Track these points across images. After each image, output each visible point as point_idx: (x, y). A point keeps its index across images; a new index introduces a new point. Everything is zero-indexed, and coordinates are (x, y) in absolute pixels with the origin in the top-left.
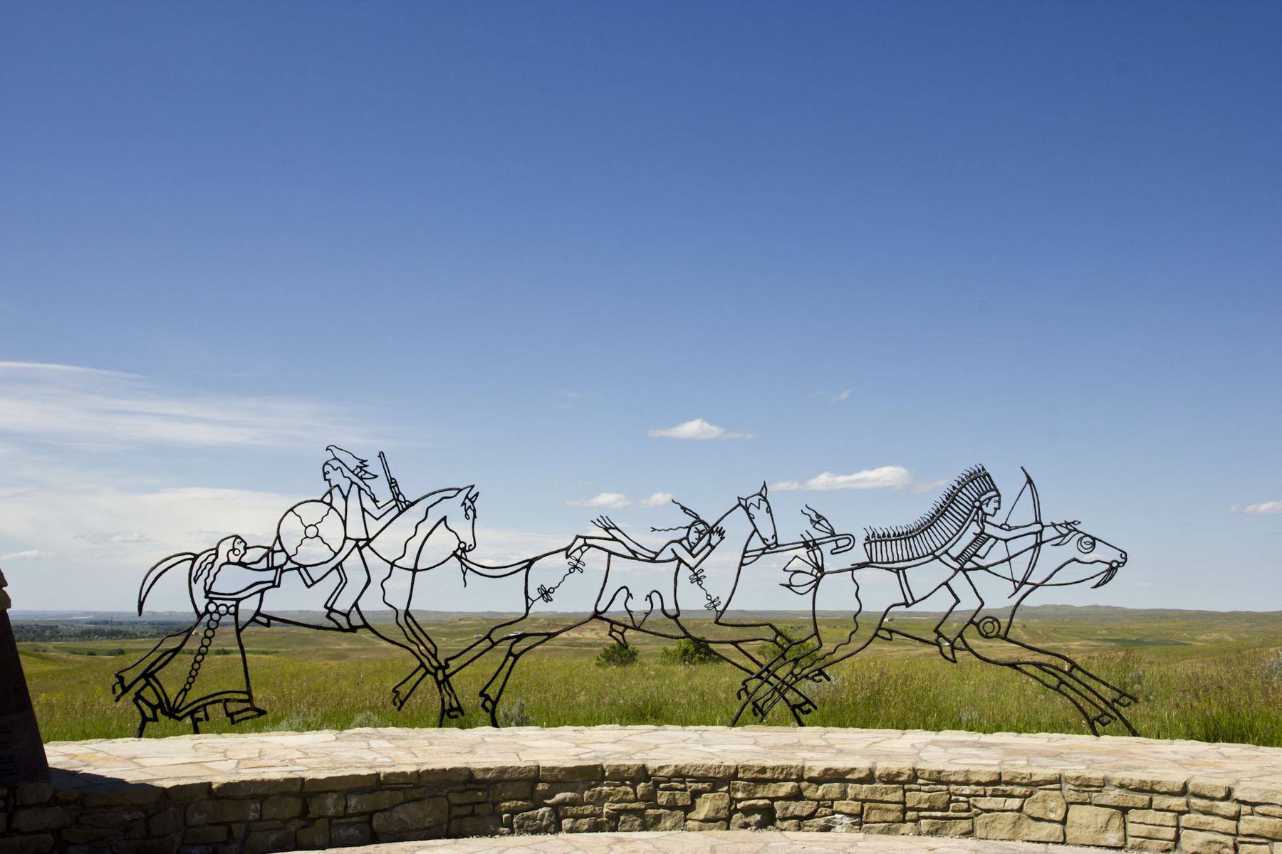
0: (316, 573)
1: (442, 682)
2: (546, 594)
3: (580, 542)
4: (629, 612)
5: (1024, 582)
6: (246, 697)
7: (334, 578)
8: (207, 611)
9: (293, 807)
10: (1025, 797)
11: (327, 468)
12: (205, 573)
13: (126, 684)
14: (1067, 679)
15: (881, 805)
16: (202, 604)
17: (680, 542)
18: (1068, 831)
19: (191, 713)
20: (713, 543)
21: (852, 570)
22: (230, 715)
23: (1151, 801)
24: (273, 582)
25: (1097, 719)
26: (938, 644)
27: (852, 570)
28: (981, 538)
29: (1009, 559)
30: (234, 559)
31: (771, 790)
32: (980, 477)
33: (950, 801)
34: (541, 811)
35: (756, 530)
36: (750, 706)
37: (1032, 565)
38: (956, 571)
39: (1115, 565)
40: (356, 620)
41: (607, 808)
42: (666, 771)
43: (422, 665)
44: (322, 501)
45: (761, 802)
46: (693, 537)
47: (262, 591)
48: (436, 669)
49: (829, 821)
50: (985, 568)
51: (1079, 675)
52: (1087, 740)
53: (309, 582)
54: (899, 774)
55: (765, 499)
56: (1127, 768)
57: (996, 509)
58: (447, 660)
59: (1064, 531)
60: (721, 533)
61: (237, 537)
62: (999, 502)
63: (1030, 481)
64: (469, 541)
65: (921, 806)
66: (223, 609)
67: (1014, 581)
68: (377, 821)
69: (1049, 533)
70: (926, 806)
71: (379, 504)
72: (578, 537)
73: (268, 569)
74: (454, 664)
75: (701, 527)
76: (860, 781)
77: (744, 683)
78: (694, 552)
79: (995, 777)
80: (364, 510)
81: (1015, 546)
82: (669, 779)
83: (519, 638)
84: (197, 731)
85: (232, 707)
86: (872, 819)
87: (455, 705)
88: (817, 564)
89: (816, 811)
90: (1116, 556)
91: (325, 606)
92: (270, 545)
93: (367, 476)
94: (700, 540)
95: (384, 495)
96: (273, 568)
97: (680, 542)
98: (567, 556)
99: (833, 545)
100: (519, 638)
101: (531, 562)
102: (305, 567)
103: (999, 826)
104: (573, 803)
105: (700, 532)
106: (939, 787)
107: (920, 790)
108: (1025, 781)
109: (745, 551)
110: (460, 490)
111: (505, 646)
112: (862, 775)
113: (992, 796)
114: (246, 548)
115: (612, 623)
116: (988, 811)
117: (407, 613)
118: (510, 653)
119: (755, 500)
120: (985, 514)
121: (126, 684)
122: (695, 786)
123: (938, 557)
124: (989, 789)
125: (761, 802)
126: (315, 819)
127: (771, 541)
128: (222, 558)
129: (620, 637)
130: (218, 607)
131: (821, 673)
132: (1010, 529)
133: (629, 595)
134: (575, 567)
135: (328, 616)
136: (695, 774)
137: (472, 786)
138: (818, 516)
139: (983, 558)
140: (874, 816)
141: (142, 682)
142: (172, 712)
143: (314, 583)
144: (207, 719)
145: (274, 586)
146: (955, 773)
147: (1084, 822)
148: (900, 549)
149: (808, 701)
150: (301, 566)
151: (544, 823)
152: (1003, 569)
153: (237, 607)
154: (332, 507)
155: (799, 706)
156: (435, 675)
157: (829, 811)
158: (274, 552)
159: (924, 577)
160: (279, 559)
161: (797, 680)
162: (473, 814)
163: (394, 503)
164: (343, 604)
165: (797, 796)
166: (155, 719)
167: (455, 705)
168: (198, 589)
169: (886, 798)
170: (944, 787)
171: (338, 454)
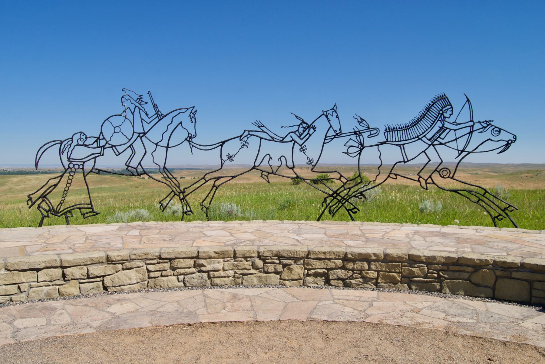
1: (183, 199)
2: (230, 158)
3: (247, 133)
4: (271, 166)
5: (462, 151)
6: (90, 206)
8: (69, 167)
10: (472, 273)
12: (67, 150)
16: (66, 163)
17: (294, 132)
20: (310, 133)
21: (378, 145)
22: (83, 215)
24: (100, 153)
25: (497, 217)
26: (419, 181)
27: (378, 145)
28: (443, 129)
29: (456, 139)
30: (81, 143)
32: (443, 98)
35: (331, 126)
37: (468, 142)
38: (430, 145)
43: (173, 191)
46: (301, 130)
47: (95, 158)
48: (180, 193)
50: (444, 144)
52: (489, 231)
53: (117, 154)
55: (336, 112)
58: (184, 189)
60: (314, 128)
61: (82, 133)
62: (452, 111)
63: (468, 100)
64: (193, 133)
67: (458, 150)
71: (149, 116)
73: (97, 147)
74: (187, 191)
75: (305, 125)
78: (302, 137)
80: (142, 119)
81: (459, 133)
83: (218, 178)
85: (84, 211)
87: (189, 209)
88: (360, 142)
90: (511, 137)
92: (98, 136)
93: (143, 103)
94: (304, 131)
95: (151, 112)
96: (100, 147)
97: (294, 132)
98: (241, 140)
99: (369, 133)
100: (218, 178)
102: (115, 146)
105: (304, 128)
109: (326, 137)
110: (188, 109)
111: (212, 182)
114: (86, 138)
117: (164, 167)
118: (214, 186)
119: (331, 112)
120: (445, 117)
123: (421, 139)
128: (75, 143)
130: (74, 165)
131: (362, 195)
132: (457, 125)
133: (270, 158)
134: (244, 145)
137: (161, 261)
138: (362, 119)
139: (443, 139)
141: (41, 200)
142: (55, 213)
143: (120, 154)
149: (355, 208)
150: (113, 146)
152: (453, 145)
155: (351, 210)
156: (179, 196)
158: (100, 140)
159: (414, 149)
160: (103, 143)
161: (350, 198)
163: (156, 116)
165: (343, 268)
166: (48, 216)
168: (64, 157)
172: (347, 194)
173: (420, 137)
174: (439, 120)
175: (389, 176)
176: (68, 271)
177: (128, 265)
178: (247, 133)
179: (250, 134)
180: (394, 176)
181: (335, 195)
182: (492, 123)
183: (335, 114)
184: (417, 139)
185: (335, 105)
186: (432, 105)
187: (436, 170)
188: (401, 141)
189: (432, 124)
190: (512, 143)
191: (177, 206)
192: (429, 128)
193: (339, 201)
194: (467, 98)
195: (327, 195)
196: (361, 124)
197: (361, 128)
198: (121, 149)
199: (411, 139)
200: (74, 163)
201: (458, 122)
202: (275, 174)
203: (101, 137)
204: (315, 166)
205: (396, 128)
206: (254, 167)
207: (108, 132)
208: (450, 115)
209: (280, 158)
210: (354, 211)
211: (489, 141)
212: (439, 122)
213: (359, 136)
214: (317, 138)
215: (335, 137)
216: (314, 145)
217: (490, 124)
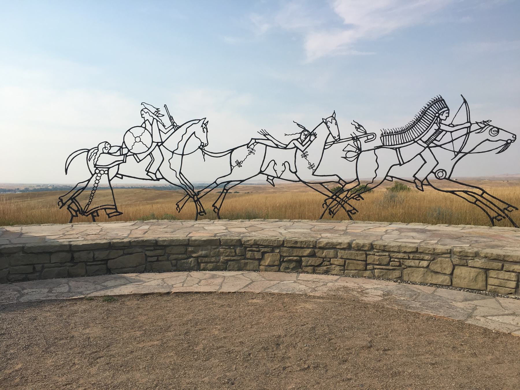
0: (141, 157)
2: (239, 164)
3: (253, 141)
5: (460, 152)
6: (114, 207)
7: (149, 158)
8: (95, 173)
9: (69, 256)
10: (431, 261)
11: (143, 112)
12: (93, 157)
13: (64, 202)
14: (479, 198)
15: (354, 261)
16: (93, 169)
17: (297, 140)
18: (454, 280)
19: (92, 213)
20: (312, 139)
21: (374, 149)
22: (108, 214)
23: (503, 266)
24: (123, 160)
25: (496, 218)
26: (414, 182)
27: (374, 149)
28: (439, 131)
29: (452, 141)
31: (300, 252)
32: (440, 101)
33: (390, 261)
34: (190, 260)
35: (330, 133)
36: (328, 211)
37: (465, 143)
38: (425, 148)
39: (509, 141)
40: (159, 176)
41: (222, 259)
42: (250, 242)
43: (188, 194)
44: (141, 126)
45: (295, 258)
46: (303, 137)
47: (119, 164)
48: (194, 196)
49: (328, 268)
50: (440, 146)
51: (485, 195)
53: (138, 161)
54: (364, 246)
55: (335, 119)
56: (493, 247)
57: (447, 117)
59: (483, 126)
60: (315, 135)
61: (106, 142)
62: (448, 113)
63: (465, 102)
64: (205, 142)
65: (375, 263)
66: (102, 172)
68: (110, 263)
69: (474, 127)
70: (377, 263)
72: (252, 139)
73: (121, 155)
75: (306, 133)
76: (344, 249)
77: (325, 201)
78: (303, 144)
79: (414, 250)
80: (159, 130)
81: (455, 135)
82: (251, 246)
84: (94, 221)
85: (109, 211)
86: (350, 268)
87: (202, 210)
88: (358, 147)
89: (322, 263)
90: (510, 137)
91: (146, 170)
92: (121, 145)
93: (160, 115)
94: (306, 138)
95: (168, 123)
96: (123, 155)
97: (297, 140)
98: (248, 147)
99: (366, 138)
100: (229, 182)
101: (233, 150)
102: (136, 154)
103: (415, 275)
104: (205, 256)
105: (306, 135)
106: (384, 254)
107: (374, 255)
108: (431, 252)
109: (326, 143)
110: (200, 120)
112: (345, 247)
113: (413, 259)
114: (110, 147)
115: (268, 175)
116: (410, 267)
117: (180, 173)
119: (330, 119)
120: (441, 120)
121: (64, 202)
122: (263, 250)
124: (411, 256)
125: (295, 258)
126: (77, 263)
127: (337, 138)
128: (100, 151)
129: (271, 182)
130: (100, 171)
132: (454, 126)
134: (251, 152)
135: (147, 174)
136: (263, 244)
137: (158, 248)
138: (359, 125)
139: (439, 141)
140: (351, 267)
141: (70, 201)
142: (83, 213)
143: (140, 161)
144: (98, 216)
145: (123, 162)
146: (393, 247)
147: (463, 275)
148: (398, 139)
149: (354, 209)
151: (192, 265)
152: (449, 146)
153: (108, 171)
154: (146, 129)
155: (350, 211)
156: (194, 198)
157: (328, 263)
158: (123, 148)
160: (125, 151)
162: (158, 260)
163: (172, 127)
164: (153, 169)
165: (313, 255)
167: (202, 210)
168: (91, 163)
169: (357, 258)
170: (387, 254)
171: (147, 106)
172: (346, 196)
173: (416, 140)
174: (435, 123)
175: (385, 179)
176: (76, 255)
177: (130, 251)
178: (253, 141)
179: (256, 141)
180: (390, 179)
181: (334, 197)
182: (490, 123)
183: (334, 121)
184: (413, 142)
185: (334, 113)
186: (429, 109)
187: (432, 172)
188: (397, 145)
189: (428, 127)
190: (511, 142)
191: (190, 206)
192: (425, 131)
193: (339, 203)
194: (464, 99)
195: (327, 197)
196: (359, 130)
197: (358, 134)
198: (141, 157)
199: (407, 142)
200: (100, 169)
201: (454, 123)
202: (279, 178)
203: (124, 146)
204: (315, 170)
205: (392, 132)
206: (261, 172)
207: (129, 141)
208: (447, 117)
209: (284, 164)
210: (353, 212)
211: (487, 141)
212: (435, 124)
213: (356, 141)
214: (318, 144)
215: (334, 143)
216: (315, 149)
217: (488, 125)
